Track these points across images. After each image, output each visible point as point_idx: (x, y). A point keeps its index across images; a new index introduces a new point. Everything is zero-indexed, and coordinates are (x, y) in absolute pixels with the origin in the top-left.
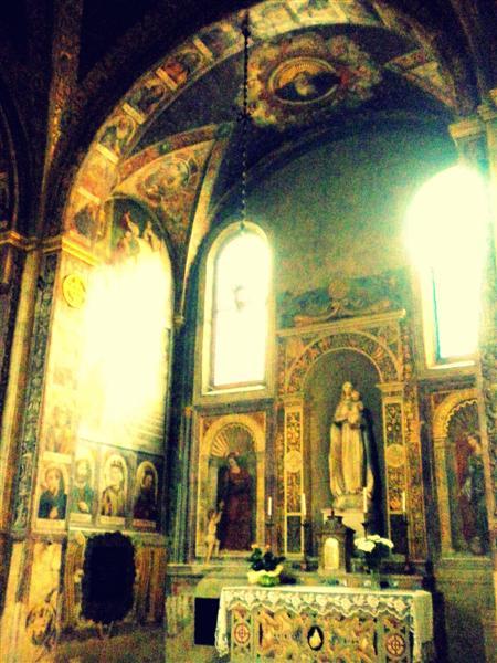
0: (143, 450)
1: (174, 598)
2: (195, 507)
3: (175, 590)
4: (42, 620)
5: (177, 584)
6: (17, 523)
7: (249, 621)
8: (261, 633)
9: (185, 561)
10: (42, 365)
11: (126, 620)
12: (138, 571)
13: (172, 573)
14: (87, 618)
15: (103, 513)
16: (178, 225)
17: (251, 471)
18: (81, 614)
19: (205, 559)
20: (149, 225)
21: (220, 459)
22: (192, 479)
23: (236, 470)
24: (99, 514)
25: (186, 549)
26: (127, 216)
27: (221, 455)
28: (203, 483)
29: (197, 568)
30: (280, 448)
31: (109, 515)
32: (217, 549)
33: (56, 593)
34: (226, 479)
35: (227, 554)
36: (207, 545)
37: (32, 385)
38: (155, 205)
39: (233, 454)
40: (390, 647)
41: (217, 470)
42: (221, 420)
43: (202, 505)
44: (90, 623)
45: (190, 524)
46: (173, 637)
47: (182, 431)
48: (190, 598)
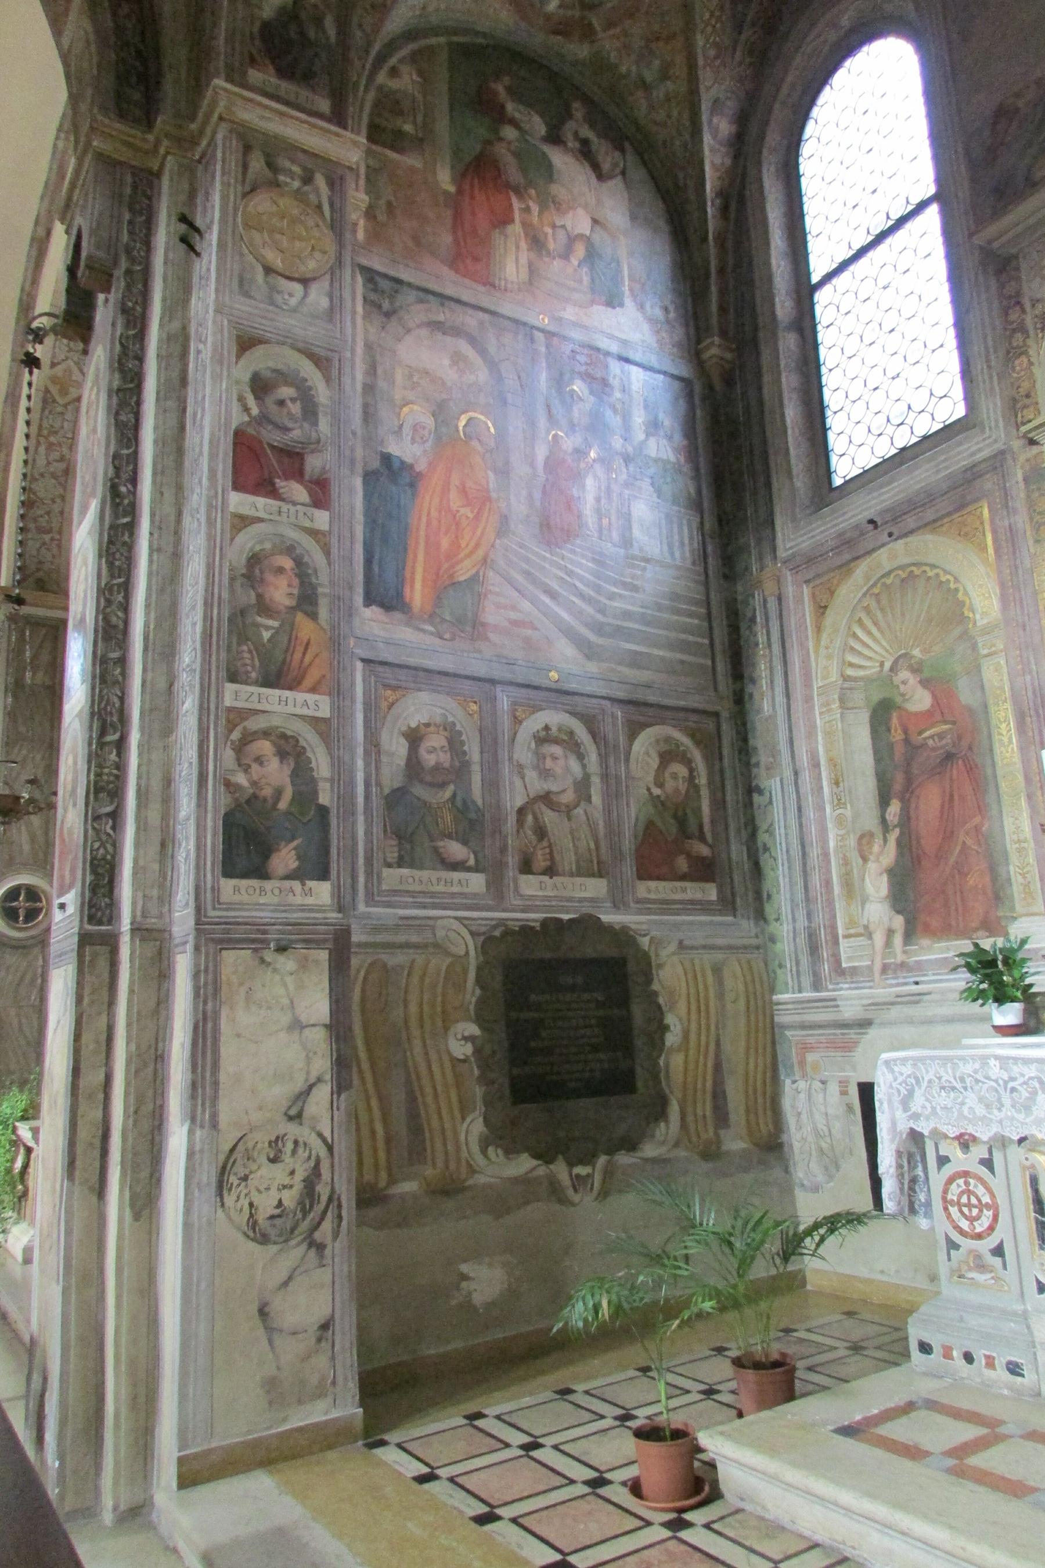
0: (640, 695)
2: (823, 830)
3: (802, 1063)
4: (278, 1174)
5: (806, 1048)
7: (988, 1163)
9: (817, 985)
11: (649, 1150)
12: (670, 1019)
14: (511, 1151)
15: (526, 867)
16: (659, 93)
17: (966, 695)
18: (484, 1144)
20: (578, 110)
22: (804, 759)
23: (920, 700)
24: (511, 872)
25: (814, 949)
26: (500, 88)
27: (871, 669)
28: (832, 762)
31: (550, 871)
32: (898, 939)
33: (323, 1093)
34: (897, 736)
38: (582, 51)
42: (862, 568)
43: (840, 821)
44: (524, 1164)
45: (816, 880)
47: (761, 638)
48: (844, 1083)
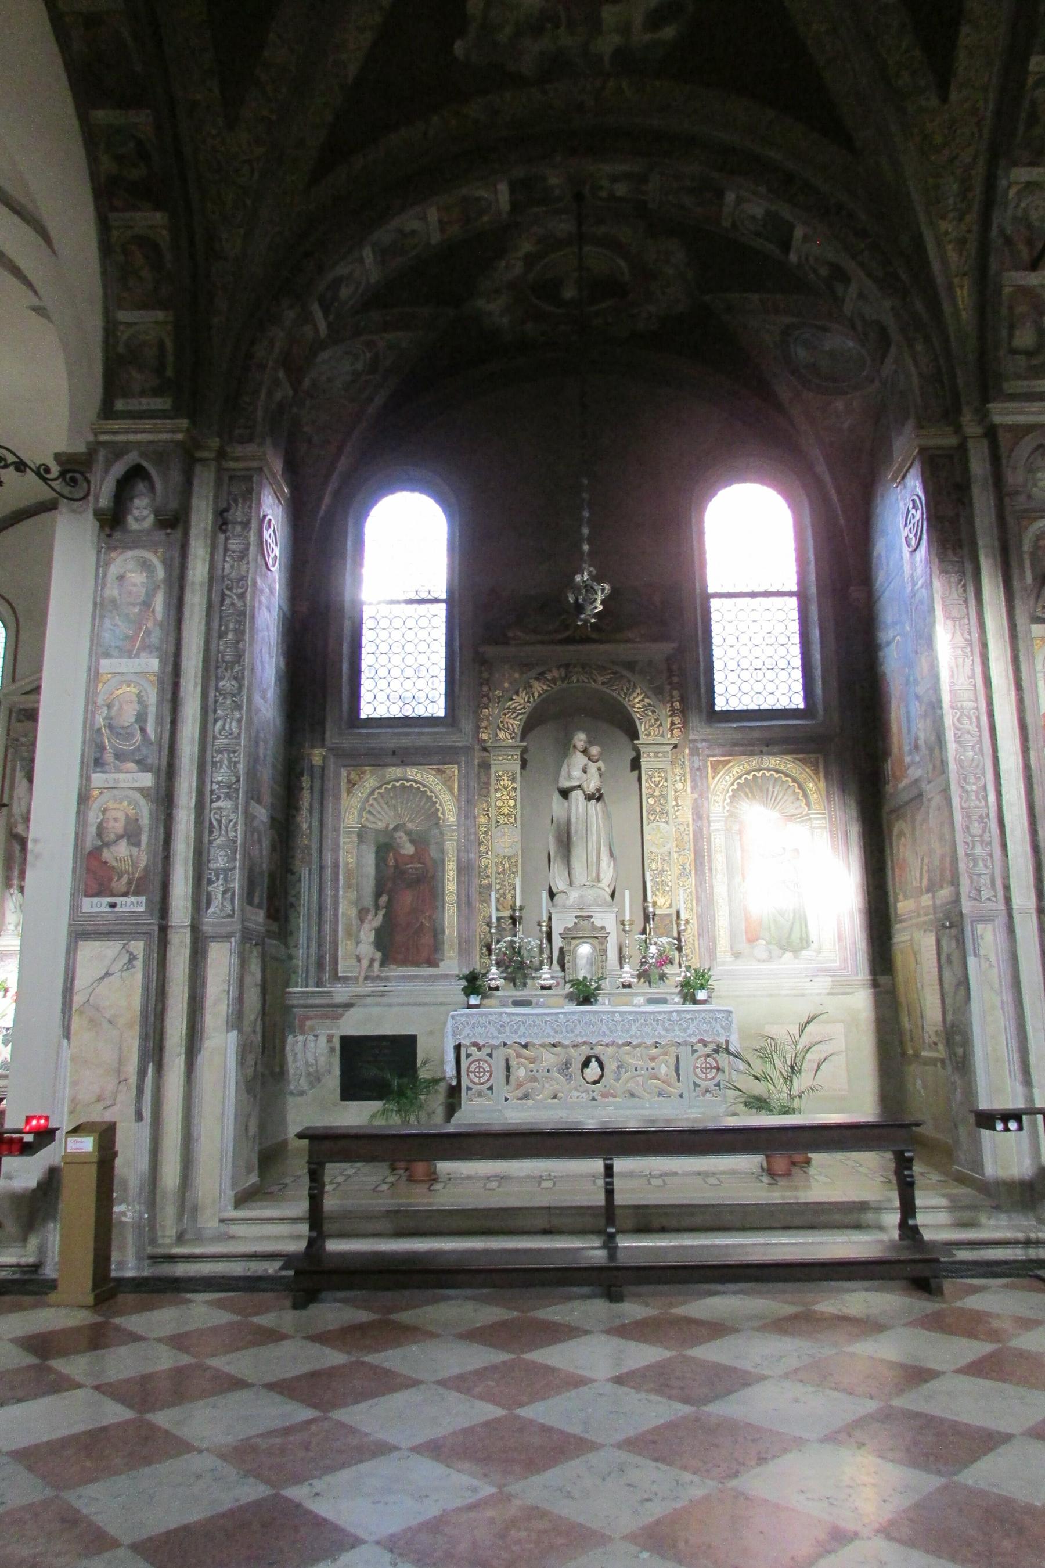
1: (300, 1038)
6: (211, 910)
8: (508, 1068)
10: (239, 657)
13: (295, 1002)
19: (356, 978)
21: (377, 832)
25: (320, 965)
27: (380, 825)
29: (341, 993)
30: (483, 820)
32: (377, 964)
35: (395, 971)
36: (359, 960)
37: (217, 689)
39: (403, 826)
40: (698, 1071)
41: (373, 849)
46: (302, 1093)
48: (330, 1039)
